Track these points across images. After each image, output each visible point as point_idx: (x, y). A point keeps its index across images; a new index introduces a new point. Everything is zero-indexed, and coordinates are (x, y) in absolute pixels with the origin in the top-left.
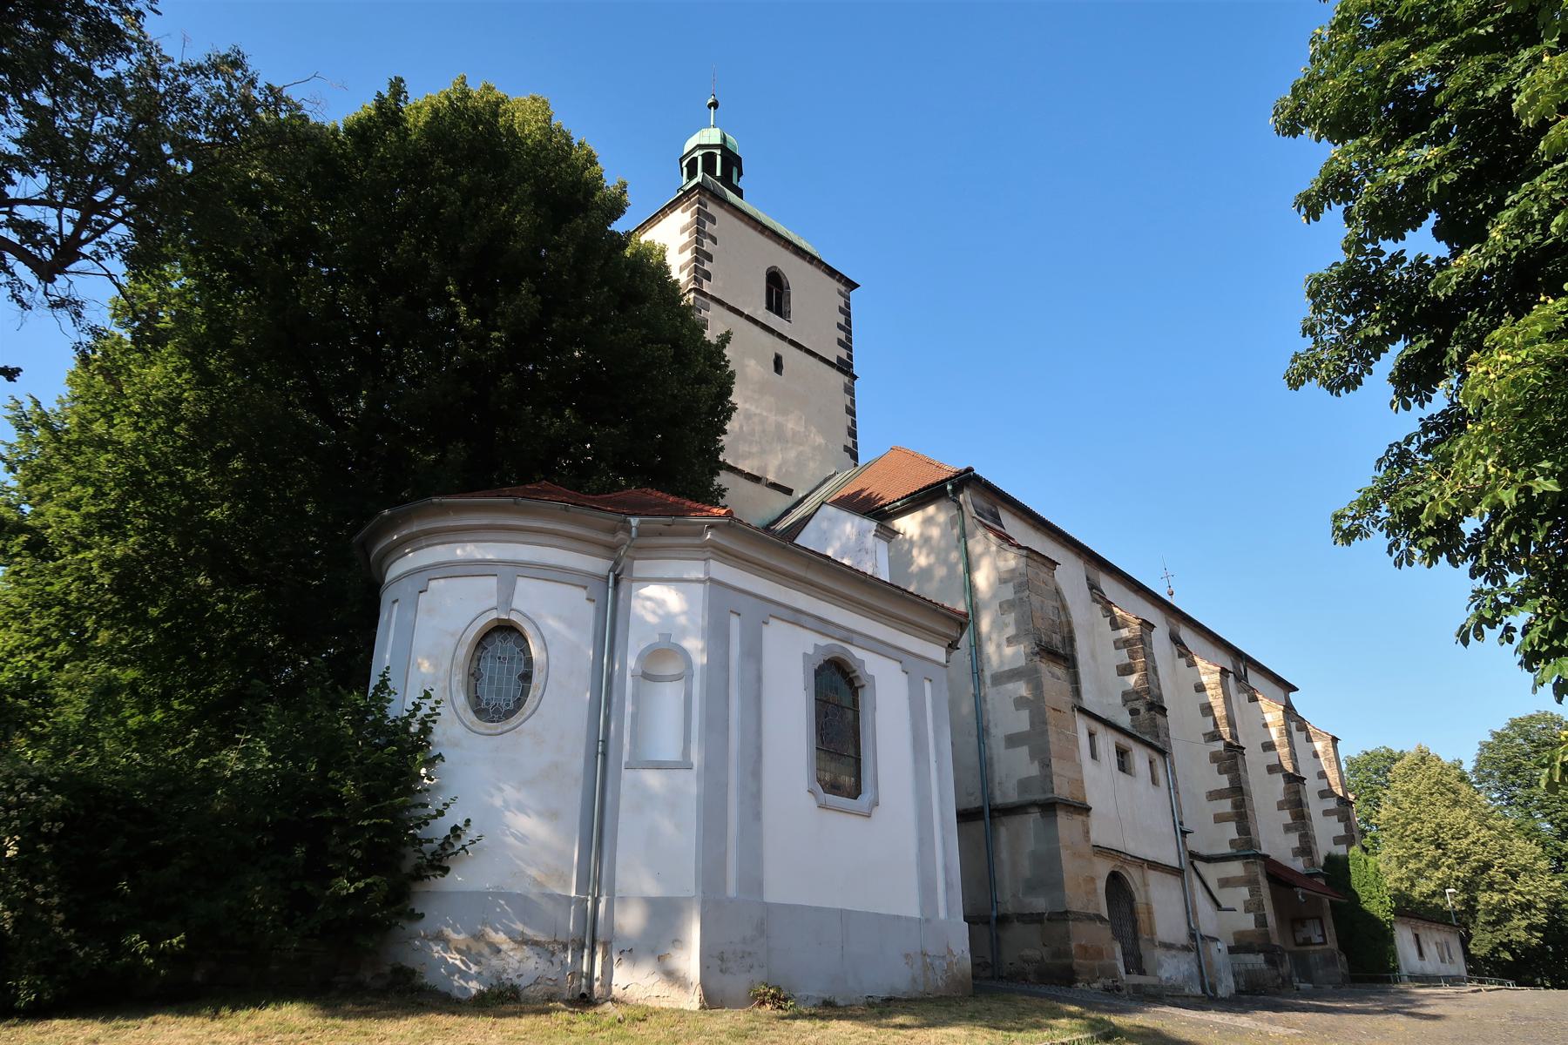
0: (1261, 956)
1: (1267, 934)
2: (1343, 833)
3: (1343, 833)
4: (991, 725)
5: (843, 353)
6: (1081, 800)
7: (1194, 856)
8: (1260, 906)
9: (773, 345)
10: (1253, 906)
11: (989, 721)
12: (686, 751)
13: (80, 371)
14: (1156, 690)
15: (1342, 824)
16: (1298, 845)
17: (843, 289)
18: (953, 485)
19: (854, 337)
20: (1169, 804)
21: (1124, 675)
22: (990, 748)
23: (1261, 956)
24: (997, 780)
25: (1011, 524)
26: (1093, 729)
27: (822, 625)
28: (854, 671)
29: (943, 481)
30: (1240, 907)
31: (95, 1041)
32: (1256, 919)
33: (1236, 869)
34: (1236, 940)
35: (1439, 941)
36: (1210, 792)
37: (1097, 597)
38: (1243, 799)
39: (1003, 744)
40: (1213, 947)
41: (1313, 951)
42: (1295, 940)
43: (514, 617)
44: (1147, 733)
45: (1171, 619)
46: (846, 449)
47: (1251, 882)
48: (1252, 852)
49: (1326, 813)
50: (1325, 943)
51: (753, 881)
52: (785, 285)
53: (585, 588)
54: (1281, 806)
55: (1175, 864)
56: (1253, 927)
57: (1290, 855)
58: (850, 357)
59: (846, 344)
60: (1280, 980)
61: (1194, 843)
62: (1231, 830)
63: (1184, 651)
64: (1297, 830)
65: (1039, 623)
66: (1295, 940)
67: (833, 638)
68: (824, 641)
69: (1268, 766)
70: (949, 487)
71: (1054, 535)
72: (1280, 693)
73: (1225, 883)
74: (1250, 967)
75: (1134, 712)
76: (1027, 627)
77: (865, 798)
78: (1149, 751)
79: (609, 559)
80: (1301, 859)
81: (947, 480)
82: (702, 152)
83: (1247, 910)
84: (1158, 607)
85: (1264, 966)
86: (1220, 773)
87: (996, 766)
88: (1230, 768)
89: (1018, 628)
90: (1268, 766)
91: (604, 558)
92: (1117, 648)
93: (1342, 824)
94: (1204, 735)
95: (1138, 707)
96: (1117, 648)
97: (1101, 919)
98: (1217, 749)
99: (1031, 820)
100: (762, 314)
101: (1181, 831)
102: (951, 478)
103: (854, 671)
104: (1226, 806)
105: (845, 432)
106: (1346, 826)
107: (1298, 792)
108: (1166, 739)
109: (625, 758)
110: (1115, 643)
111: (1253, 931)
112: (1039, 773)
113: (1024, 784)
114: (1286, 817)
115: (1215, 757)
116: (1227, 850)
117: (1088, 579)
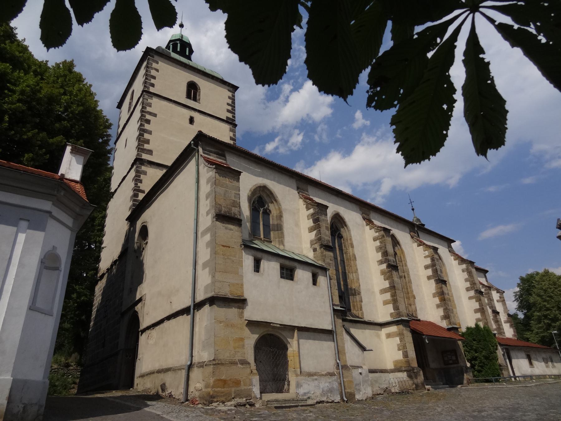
0: (405, 373)
2: (478, 307)
3: (478, 307)
5: (230, 115)
6: (239, 293)
9: (188, 113)
10: (402, 347)
16: (443, 314)
17: (231, 89)
19: (236, 109)
21: (311, 232)
23: (405, 373)
24: (198, 289)
31: (464, 418)
34: (395, 366)
35: (545, 357)
36: (381, 290)
37: (301, 196)
38: (395, 292)
39: (378, 293)
40: (355, 372)
47: (400, 335)
48: (400, 319)
49: (470, 298)
52: (198, 88)
55: (329, 327)
56: (402, 358)
57: (439, 319)
58: (234, 117)
59: (232, 111)
60: (414, 386)
62: (390, 308)
64: (442, 307)
65: (221, 202)
69: (427, 276)
71: (271, 167)
75: (315, 250)
82: (171, 43)
84: (354, 203)
86: (385, 280)
88: (389, 277)
90: (427, 276)
92: (308, 219)
94: (378, 262)
96: (308, 219)
97: (244, 362)
100: (183, 100)
104: (388, 296)
106: (479, 304)
110: (308, 217)
111: (401, 360)
114: (437, 300)
115: (383, 273)
116: (389, 319)
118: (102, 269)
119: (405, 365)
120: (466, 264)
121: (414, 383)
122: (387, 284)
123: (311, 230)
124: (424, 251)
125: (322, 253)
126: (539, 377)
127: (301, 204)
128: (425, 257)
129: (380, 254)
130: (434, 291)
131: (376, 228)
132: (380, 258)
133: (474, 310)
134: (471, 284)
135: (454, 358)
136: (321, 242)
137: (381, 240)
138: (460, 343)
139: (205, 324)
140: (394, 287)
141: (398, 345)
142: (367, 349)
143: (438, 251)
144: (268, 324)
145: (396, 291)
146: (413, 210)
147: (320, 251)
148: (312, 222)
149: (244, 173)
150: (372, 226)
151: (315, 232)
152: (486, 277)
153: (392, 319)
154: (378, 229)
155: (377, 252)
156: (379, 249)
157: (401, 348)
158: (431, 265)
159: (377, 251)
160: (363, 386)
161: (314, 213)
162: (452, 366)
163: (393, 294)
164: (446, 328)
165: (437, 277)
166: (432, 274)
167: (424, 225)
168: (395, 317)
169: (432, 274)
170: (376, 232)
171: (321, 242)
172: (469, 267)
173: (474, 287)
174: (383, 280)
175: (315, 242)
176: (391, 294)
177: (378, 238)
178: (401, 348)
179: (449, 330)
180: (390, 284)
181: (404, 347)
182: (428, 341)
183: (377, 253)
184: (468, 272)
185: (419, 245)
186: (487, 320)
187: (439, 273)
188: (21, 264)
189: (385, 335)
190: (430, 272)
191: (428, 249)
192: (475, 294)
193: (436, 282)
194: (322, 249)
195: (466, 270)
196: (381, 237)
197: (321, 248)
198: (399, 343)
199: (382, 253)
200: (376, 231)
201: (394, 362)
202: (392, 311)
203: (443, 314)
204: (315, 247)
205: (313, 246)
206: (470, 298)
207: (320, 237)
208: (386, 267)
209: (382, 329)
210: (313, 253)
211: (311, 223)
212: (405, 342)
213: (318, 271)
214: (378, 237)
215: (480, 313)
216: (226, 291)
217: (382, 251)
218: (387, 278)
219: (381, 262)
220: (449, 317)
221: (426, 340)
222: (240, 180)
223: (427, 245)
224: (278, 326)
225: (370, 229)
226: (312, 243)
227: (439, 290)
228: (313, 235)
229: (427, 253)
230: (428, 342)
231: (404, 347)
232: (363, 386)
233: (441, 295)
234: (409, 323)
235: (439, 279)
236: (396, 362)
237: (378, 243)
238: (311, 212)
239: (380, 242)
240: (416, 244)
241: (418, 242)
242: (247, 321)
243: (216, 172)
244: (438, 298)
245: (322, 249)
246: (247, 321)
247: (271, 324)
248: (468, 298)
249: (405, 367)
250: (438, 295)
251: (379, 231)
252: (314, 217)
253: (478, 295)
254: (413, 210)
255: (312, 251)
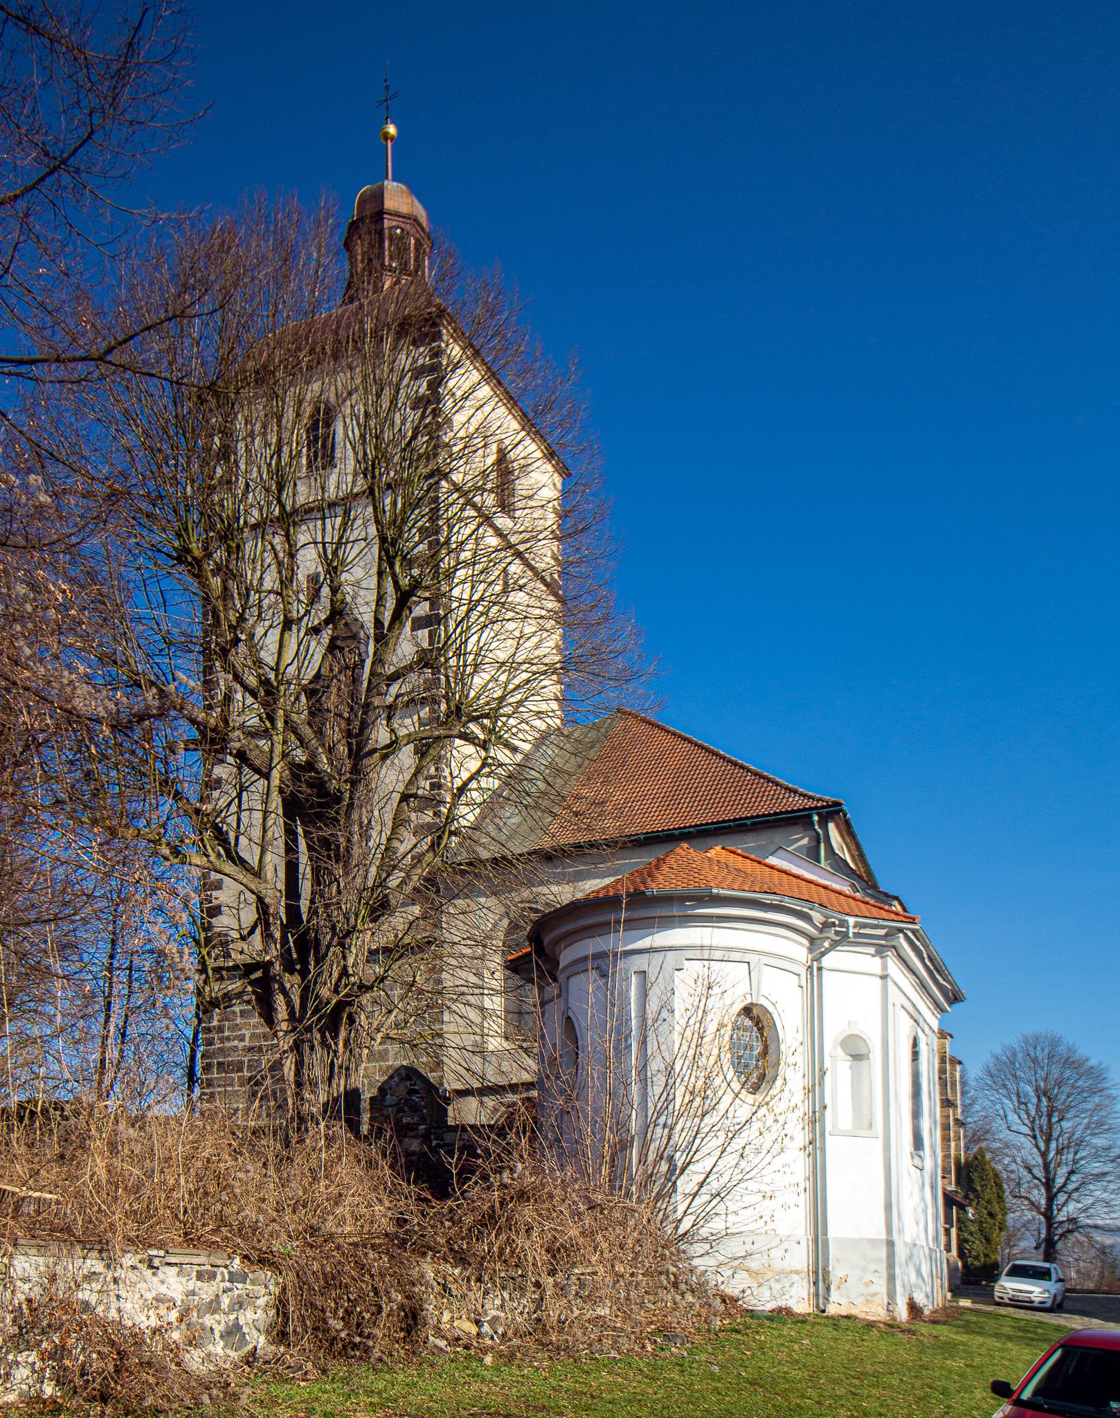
18: (818, 814)
43: (762, 1001)
70: (816, 818)
152: (815, 971)
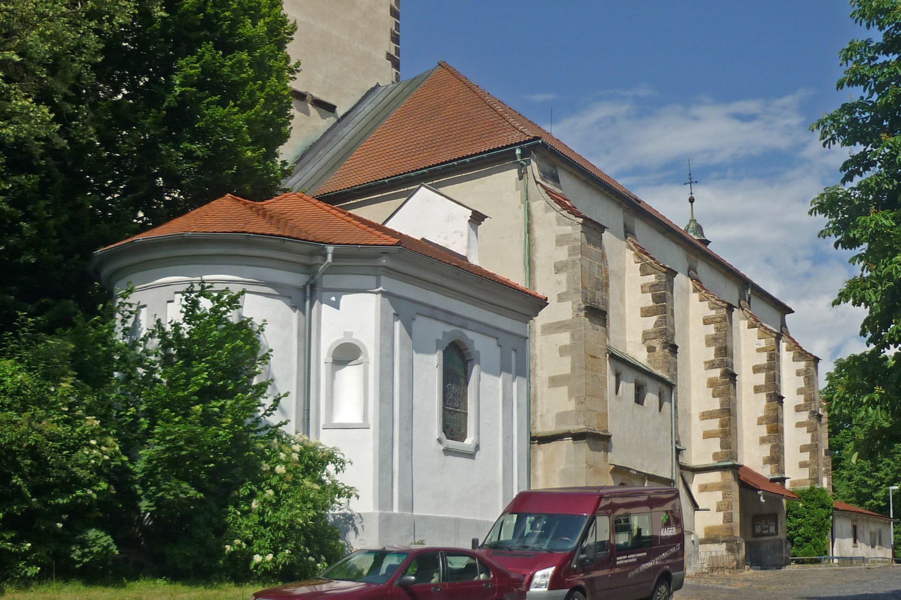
0: (724, 545)
1: (731, 529)
2: (809, 442)
3: (809, 442)
4: (538, 368)
7: (683, 468)
8: (729, 506)
11: (536, 364)
12: (365, 416)
13: (741, 562)
14: (671, 330)
15: (810, 435)
16: (769, 455)
18: (521, 149)
20: (670, 426)
21: (646, 316)
22: (535, 387)
23: (395, 322)
24: (539, 414)
25: (569, 185)
26: (619, 370)
27: (448, 317)
28: (467, 349)
29: (512, 145)
30: (713, 508)
32: (725, 517)
33: (715, 477)
37: (631, 244)
38: (730, 418)
39: (547, 383)
41: (766, 541)
42: (754, 530)
44: (659, 368)
45: (691, 256)
46: (389, 57)
47: (723, 487)
48: (730, 463)
49: (799, 425)
50: (777, 533)
51: (408, 504)
53: (290, 298)
54: (760, 422)
57: (761, 463)
60: (735, 563)
61: (684, 460)
62: (715, 445)
63: (698, 287)
64: (770, 442)
66: (754, 530)
67: (455, 325)
68: (449, 329)
69: (755, 387)
70: (518, 152)
72: (776, 315)
73: (704, 488)
74: (714, 554)
75: (651, 349)
76: (576, 286)
77: (470, 441)
78: (660, 385)
79: (306, 274)
80: (769, 466)
81: (516, 144)
83: (719, 510)
85: (725, 553)
86: (714, 396)
87: (539, 402)
88: (723, 393)
89: (569, 286)
90: (755, 387)
91: (302, 273)
92: (643, 292)
93: (810, 435)
94: (706, 363)
95: (654, 345)
96: (643, 292)
98: (714, 376)
99: (565, 445)
101: (676, 449)
102: (520, 143)
103: (467, 349)
104: (714, 424)
105: (387, 37)
106: (813, 436)
107: (777, 409)
108: (674, 372)
109: (322, 421)
110: (642, 287)
111: (721, 526)
112: (574, 409)
113: (561, 417)
114: (763, 431)
115: (712, 383)
116: (710, 461)
117: (625, 226)
118: (264, 350)
119: (725, 534)
120: (806, 361)
121: (735, 559)
122: (716, 404)
123: (646, 313)
124: (759, 339)
125: (665, 356)
126: (863, 559)
127: (630, 256)
128: (759, 350)
129: (712, 350)
130: (762, 414)
131: (713, 300)
132: (712, 357)
133: (801, 446)
134: (806, 400)
135: (772, 530)
136: (665, 338)
137: (718, 325)
138: (784, 501)
139: (562, 467)
140: (729, 410)
141: (718, 503)
142: (700, 508)
143: (819, 364)
144: (628, 470)
145: (731, 417)
146: (692, 200)
147: (661, 353)
148: (651, 299)
149: (680, 274)
150: (706, 295)
151: (655, 318)
153: (716, 462)
154: (716, 304)
155: (708, 344)
156: (710, 341)
157: (722, 508)
158: (766, 367)
159: (706, 343)
160: (694, 557)
161: (657, 285)
162: (766, 538)
163: (725, 423)
164: (769, 478)
165: (772, 390)
166: (764, 383)
167: (707, 242)
168: (721, 460)
169: (764, 383)
170: (712, 309)
171: (665, 338)
172: (811, 368)
173: (811, 406)
174: (711, 396)
175: (652, 336)
176: (720, 422)
177: (715, 320)
178: (723, 507)
179: (773, 481)
180: (721, 405)
181: (728, 506)
182: (764, 499)
183: (707, 346)
184: (806, 377)
185: (751, 326)
186: (818, 466)
187: (777, 383)
188: (519, 406)
189: (697, 487)
190: (761, 379)
191: (766, 336)
192: (809, 418)
193: (768, 398)
194: (667, 350)
195: (803, 373)
196: (719, 319)
197: (664, 348)
198: (721, 500)
199: (716, 350)
200: (712, 306)
201: (705, 529)
202: (718, 449)
203: (769, 455)
204: (652, 344)
205: (648, 342)
206: (799, 425)
207: (666, 328)
208: (719, 376)
209: (696, 475)
210: (647, 353)
211: (648, 300)
212: (731, 499)
213: (650, 384)
214: (714, 318)
215: (704, 537)
216: (594, 426)
217: (718, 345)
218: (719, 394)
219: (711, 365)
220: (778, 460)
221: (762, 498)
222: (751, 329)
223: (766, 328)
224: (635, 473)
225: (700, 301)
226: (646, 336)
227: (771, 414)
228: (651, 322)
229: (763, 343)
230: (764, 501)
231: (728, 506)
232: (694, 557)
233: (773, 422)
234: (738, 469)
235: (775, 394)
236: (709, 530)
237: (711, 330)
238: (651, 281)
239: (717, 328)
240: (746, 322)
241: (751, 319)
242: (613, 466)
243: (582, 232)
244: (766, 425)
245: (667, 350)
246: (613, 466)
247: (631, 471)
248: (794, 424)
249: (723, 537)
250: (767, 421)
251: (719, 308)
252: (656, 291)
253: (815, 421)
254: (692, 200)
255: (646, 350)
